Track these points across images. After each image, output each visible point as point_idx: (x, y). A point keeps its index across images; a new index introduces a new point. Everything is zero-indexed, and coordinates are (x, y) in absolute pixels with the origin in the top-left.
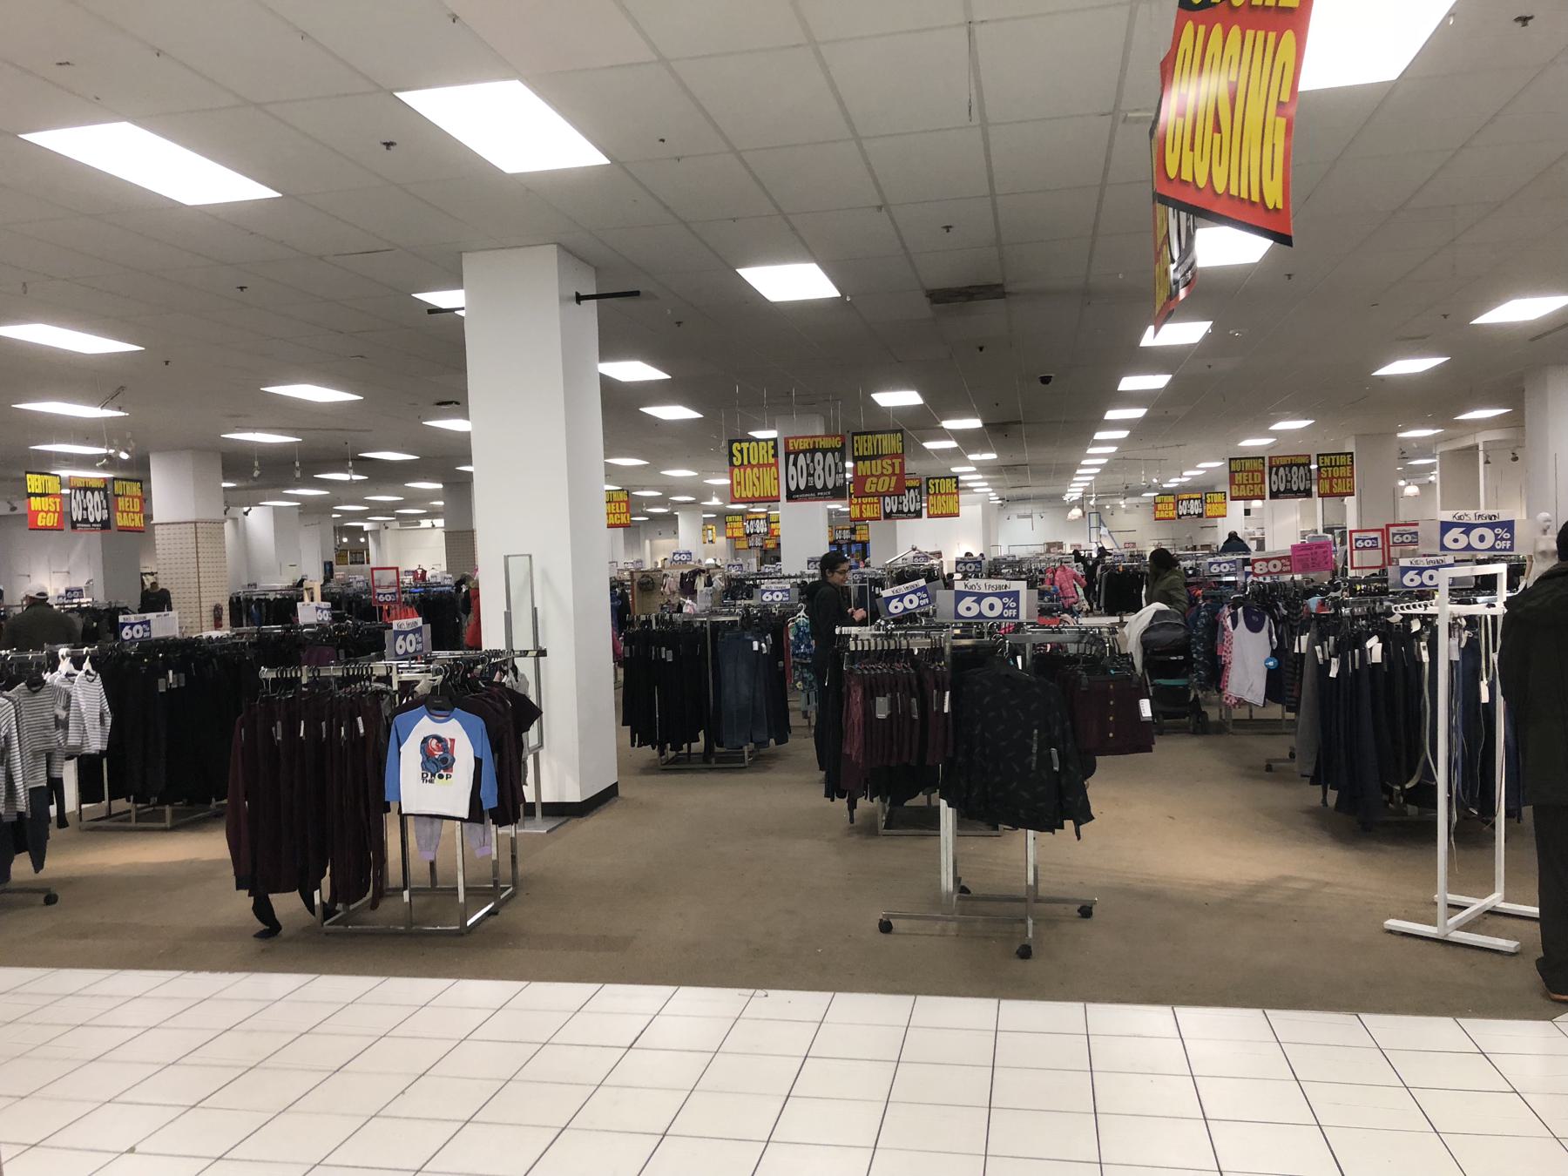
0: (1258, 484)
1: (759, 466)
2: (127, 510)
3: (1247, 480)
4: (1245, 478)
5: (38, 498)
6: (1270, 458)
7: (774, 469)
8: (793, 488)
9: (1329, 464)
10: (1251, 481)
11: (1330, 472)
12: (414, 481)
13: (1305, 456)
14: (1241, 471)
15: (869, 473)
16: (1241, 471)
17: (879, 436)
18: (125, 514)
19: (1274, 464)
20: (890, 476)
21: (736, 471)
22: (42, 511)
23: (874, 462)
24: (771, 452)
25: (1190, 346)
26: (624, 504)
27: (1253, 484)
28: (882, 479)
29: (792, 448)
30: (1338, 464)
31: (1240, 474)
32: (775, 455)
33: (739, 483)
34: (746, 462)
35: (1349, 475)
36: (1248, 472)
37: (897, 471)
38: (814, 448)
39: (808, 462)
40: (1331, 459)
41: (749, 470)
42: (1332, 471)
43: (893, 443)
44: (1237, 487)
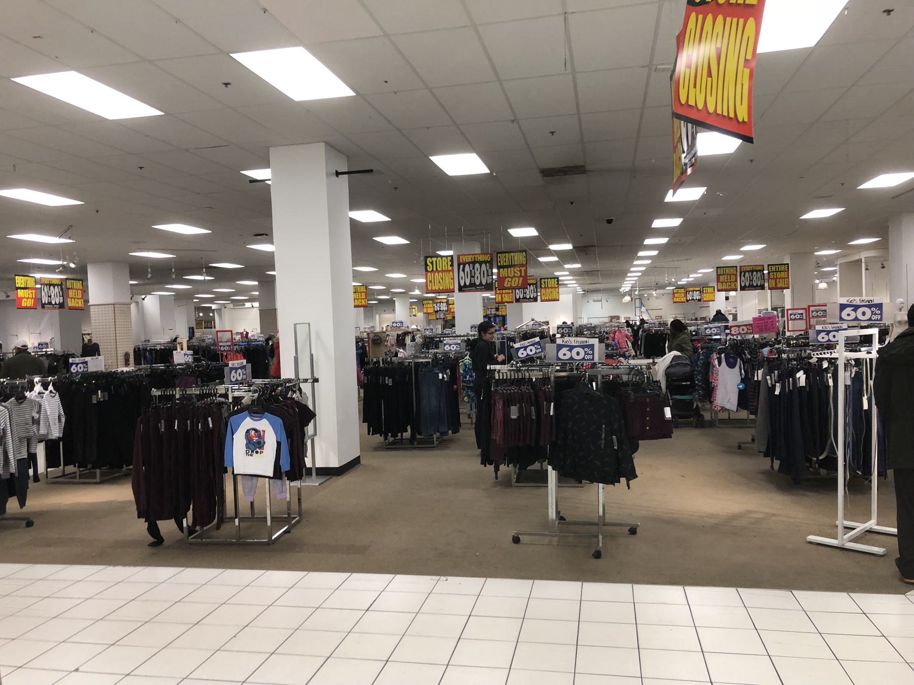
0: (733, 282)
1: (442, 271)
2: (74, 297)
3: (727, 280)
4: (726, 278)
5: (22, 290)
6: (740, 267)
7: (451, 273)
8: (462, 284)
9: (775, 270)
10: (729, 280)
11: (775, 275)
12: (241, 280)
13: (761, 265)
14: (723, 274)
15: (506, 276)
16: (723, 274)
17: (512, 254)
18: (73, 300)
19: (742, 270)
20: (519, 277)
21: (429, 274)
22: (25, 298)
23: (509, 269)
24: (450, 263)
25: (694, 202)
26: (364, 294)
27: (731, 282)
28: (514, 279)
29: (461, 261)
30: (780, 270)
31: (723, 276)
32: (452, 265)
33: (431, 282)
34: (435, 269)
35: (786, 277)
36: (728, 275)
37: (523, 275)
38: (475, 261)
39: (471, 269)
40: (776, 267)
41: (436, 274)
42: (776, 274)
43: (521, 258)
44: (721, 284)
